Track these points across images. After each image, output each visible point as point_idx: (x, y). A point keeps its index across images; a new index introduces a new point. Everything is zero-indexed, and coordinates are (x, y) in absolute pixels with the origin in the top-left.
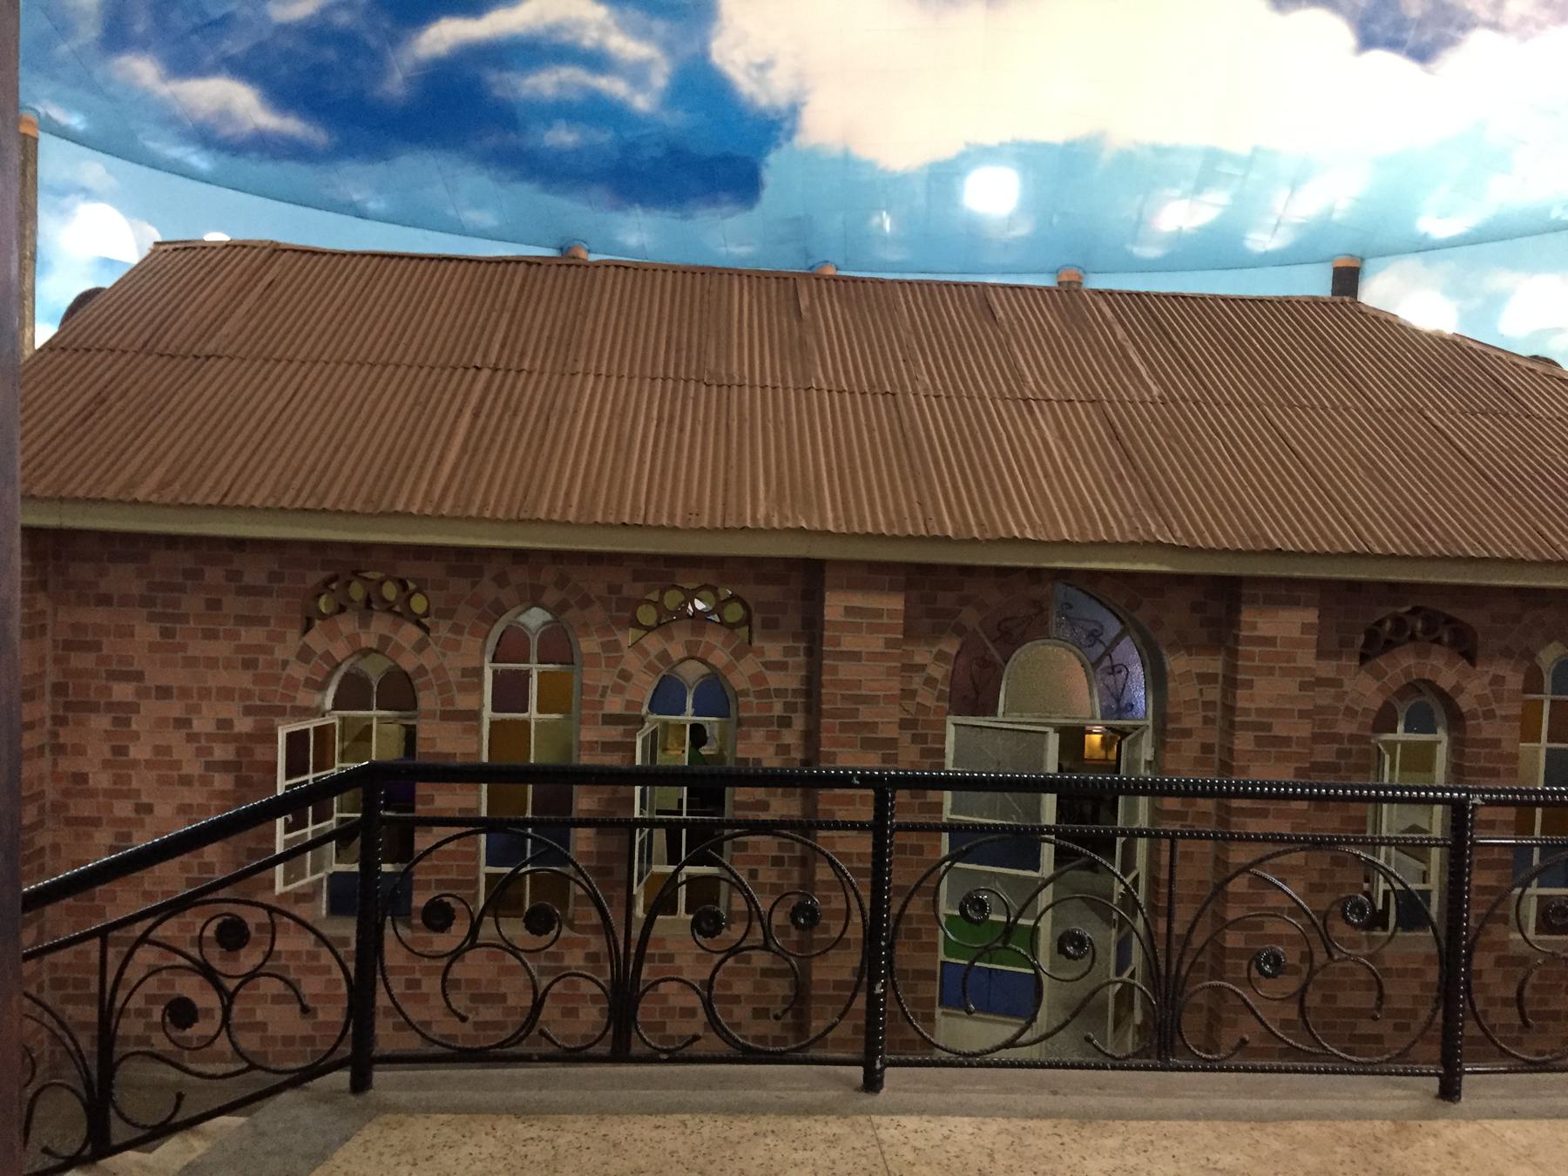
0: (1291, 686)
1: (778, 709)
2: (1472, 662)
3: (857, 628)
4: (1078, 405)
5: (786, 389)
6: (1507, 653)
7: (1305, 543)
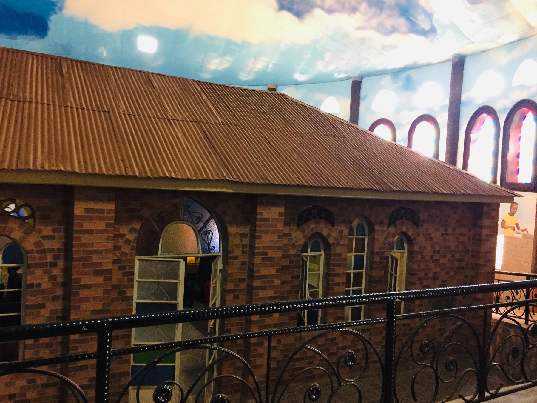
0: (275, 237)
1: (50, 258)
2: (333, 226)
3: (91, 218)
4: (190, 123)
5: (54, 105)
6: (344, 222)
7: (281, 181)
